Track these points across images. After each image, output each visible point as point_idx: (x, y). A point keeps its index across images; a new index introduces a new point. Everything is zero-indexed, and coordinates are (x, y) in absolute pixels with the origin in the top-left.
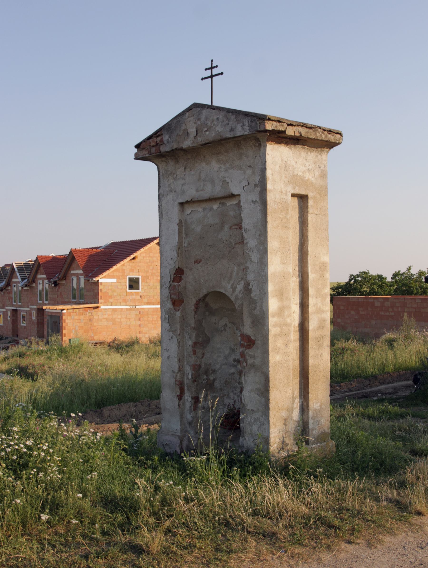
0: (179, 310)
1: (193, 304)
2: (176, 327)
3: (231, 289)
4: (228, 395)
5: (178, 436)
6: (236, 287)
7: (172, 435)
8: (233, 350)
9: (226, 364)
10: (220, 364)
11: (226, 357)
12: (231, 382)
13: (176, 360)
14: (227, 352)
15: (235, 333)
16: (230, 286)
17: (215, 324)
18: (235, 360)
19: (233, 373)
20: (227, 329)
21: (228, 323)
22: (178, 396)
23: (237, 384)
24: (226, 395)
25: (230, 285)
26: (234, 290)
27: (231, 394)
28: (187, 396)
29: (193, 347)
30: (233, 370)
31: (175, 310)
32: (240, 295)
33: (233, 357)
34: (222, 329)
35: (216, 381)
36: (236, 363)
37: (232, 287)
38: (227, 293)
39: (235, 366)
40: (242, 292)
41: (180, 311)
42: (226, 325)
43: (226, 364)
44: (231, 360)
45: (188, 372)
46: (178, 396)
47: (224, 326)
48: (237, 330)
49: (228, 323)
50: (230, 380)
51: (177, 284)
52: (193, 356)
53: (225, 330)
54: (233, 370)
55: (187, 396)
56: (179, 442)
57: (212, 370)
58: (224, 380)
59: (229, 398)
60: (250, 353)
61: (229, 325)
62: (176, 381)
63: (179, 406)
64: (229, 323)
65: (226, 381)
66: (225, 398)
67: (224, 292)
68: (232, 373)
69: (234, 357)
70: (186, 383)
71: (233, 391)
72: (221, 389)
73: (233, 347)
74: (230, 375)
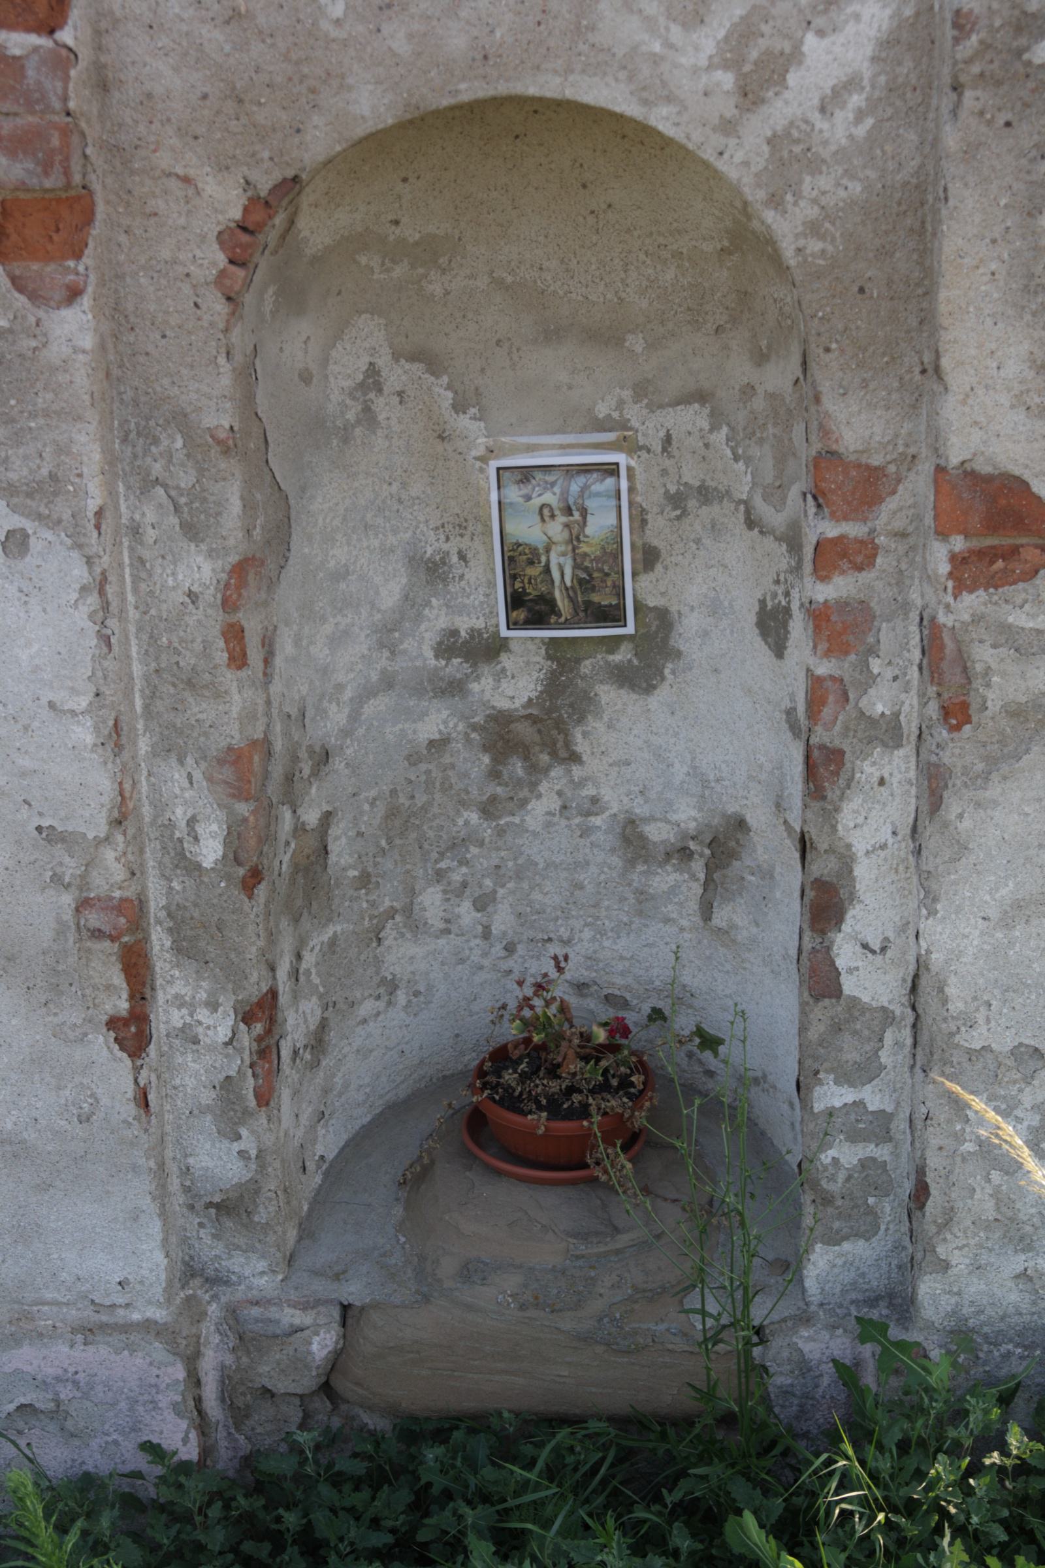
0: (74, 294)
1: (212, 229)
2: (62, 450)
3: (726, 80)
4: (408, 911)
5: (147, 1326)
6: (795, 56)
7: (88, 1332)
8: (433, 572)
9: (388, 682)
10: (348, 694)
11: (387, 636)
12: (424, 809)
13: (84, 734)
14: (390, 594)
15: (441, 438)
16: (709, 47)
17: (306, 378)
18: (449, 645)
19: (438, 745)
20: (384, 407)
21: (383, 360)
22: (113, 1023)
23: (474, 817)
24: (391, 913)
25: (708, 41)
26: (759, 75)
27: (431, 900)
28: (179, 1001)
29: (228, 604)
30: (436, 720)
31: (34, 297)
32: (841, 129)
33: (439, 618)
34: (351, 416)
35: (334, 831)
36: (456, 667)
37: (733, 51)
38: (662, 119)
39: (454, 688)
40: (856, 100)
41: (86, 301)
42: (372, 380)
43: (388, 682)
44: (420, 648)
45: (180, 814)
46: (113, 1023)
47: (362, 385)
48: (459, 407)
49: (383, 360)
50: (421, 799)
51: (34, 39)
52: (229, 678)
53: (368, 416)
54: (436, 720)
55: (179, 1001)
56: (179, 1372)
57: (311, 751)
58: (381, 809)
59: (415, 925)
60: (1018, 619)
61: (395, 376)
62: (83, 905)
63: (143, 1099)
64: (396, 356)
65: (393, 813)
66: (389, 933)
67: (629, 108)
68: (431, 743)
69: (443, 622)
70: (156, 902)
71: (440, 875)
72: (364, 880)
73: (432, 546)
74: (413, 759)
